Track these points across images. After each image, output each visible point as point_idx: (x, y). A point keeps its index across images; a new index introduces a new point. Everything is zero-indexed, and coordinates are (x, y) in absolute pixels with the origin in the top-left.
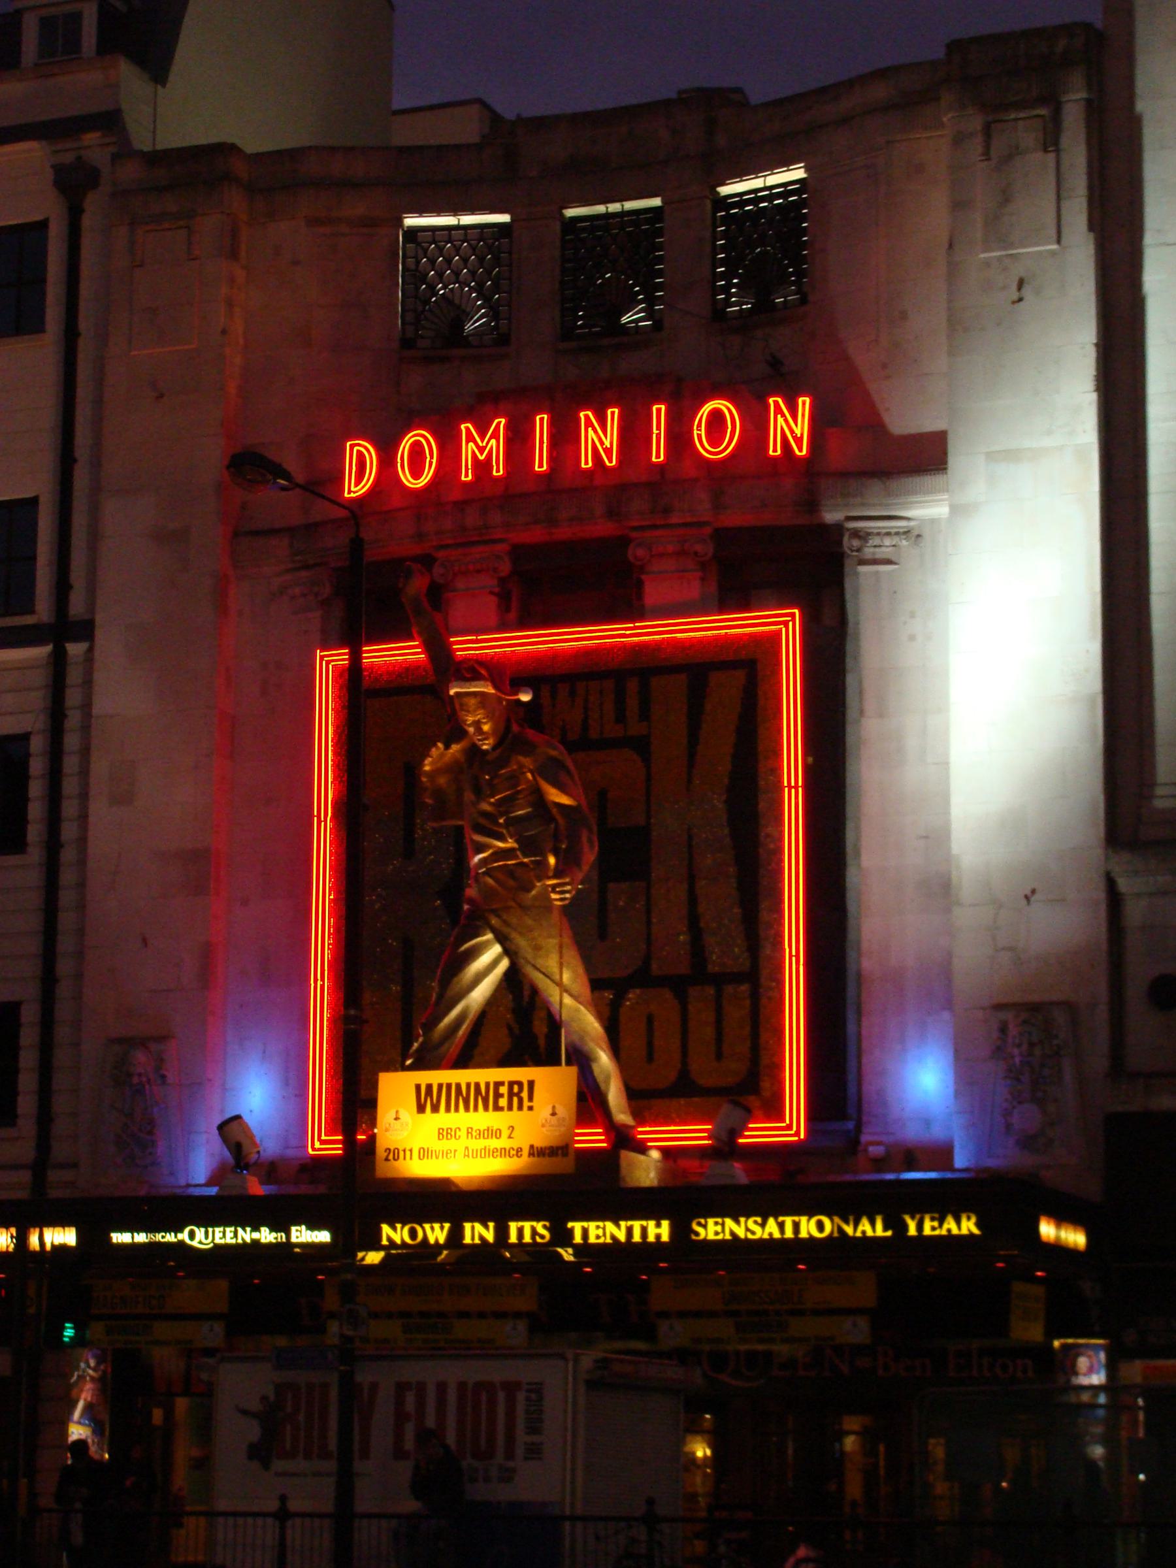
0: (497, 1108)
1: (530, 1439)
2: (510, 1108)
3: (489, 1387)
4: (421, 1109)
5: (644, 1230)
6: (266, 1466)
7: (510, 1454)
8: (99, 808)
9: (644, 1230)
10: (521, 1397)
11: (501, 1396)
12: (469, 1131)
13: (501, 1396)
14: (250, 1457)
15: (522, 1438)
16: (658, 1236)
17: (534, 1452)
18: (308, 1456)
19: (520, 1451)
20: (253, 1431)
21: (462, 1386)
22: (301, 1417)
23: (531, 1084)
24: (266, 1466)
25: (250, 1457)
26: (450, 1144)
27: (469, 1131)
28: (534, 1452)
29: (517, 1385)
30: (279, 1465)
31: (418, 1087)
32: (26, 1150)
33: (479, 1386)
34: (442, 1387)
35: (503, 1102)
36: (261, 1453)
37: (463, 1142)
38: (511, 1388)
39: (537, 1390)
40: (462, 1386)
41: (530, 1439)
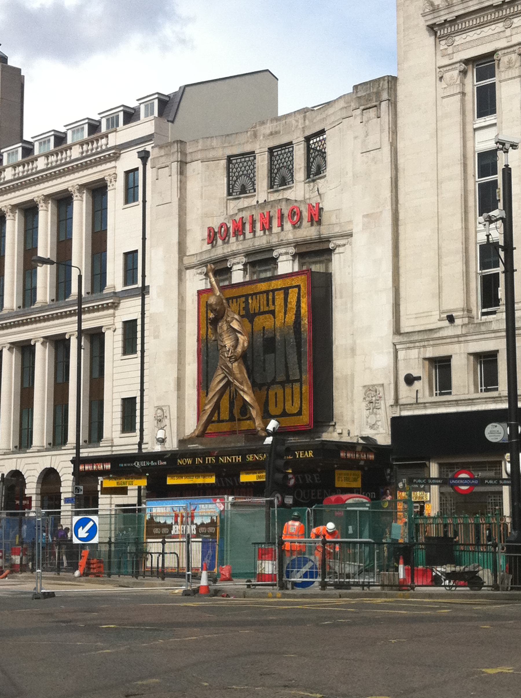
5: (235, 458)
9: (235, 458)
32: (137, 440)
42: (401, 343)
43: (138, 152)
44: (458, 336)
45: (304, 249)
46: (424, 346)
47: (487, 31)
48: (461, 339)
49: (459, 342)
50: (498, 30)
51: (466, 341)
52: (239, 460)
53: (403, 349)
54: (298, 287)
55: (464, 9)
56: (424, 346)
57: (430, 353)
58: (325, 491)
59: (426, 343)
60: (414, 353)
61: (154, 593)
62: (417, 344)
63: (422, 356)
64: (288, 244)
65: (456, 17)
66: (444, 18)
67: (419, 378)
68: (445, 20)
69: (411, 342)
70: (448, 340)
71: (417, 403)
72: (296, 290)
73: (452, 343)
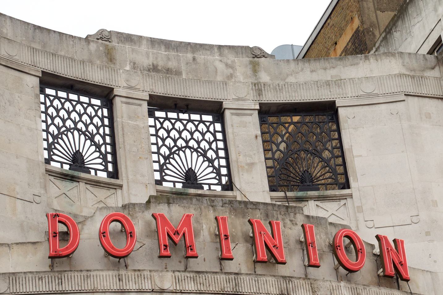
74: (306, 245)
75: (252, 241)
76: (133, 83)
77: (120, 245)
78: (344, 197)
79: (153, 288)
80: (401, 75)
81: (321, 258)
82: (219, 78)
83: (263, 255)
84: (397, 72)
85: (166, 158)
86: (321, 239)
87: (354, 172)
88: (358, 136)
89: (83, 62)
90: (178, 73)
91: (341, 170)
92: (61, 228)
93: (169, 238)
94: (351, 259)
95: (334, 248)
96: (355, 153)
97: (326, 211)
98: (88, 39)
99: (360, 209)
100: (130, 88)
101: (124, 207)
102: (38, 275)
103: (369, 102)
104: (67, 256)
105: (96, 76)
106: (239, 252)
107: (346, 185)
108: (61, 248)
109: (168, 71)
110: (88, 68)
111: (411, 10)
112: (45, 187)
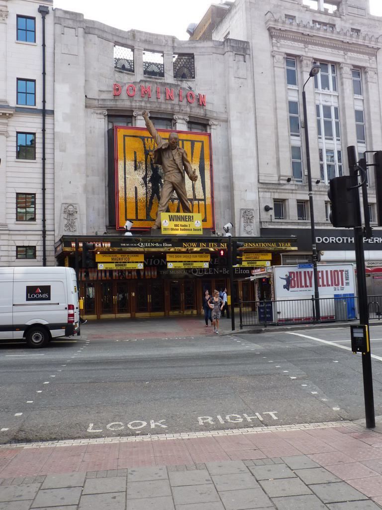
0: (186, 221)
1: (346, 281)
2: (189, 221)
3: (337, 271)
4: (170, 220)
5: (347, 240)
6: (288, 289)
7: (342, 285)
8: (57, 153)
9: (347, 240)
10: (344, 273)
11: (340, 273)
12: (181, 225)
13: (340, 273)
14: (284, 288)
15: (345, 281)
16: (351, 241)
17: (347, 284)
18: (298, 287)
19: (345, 284)
20: (285, 282)
21: (331, 271)
22: (296, 279)
23: (193, 216)
24: (288, 289)
25: (284, 288)
26: (177, 228)
27: (181, 225)
28: (347, 284)
29: (343, 271)
30: (291, 289)
31: (169, 216)
32: (40, 227)
33: (335, 271)
34: (327, 272)
35: (187, 220)
36: (287, 287)
37: (179, 228)
38: (342, 271)
39: (347, 271)
40: (331, 271)
41: (346, 281)
42: (262, 188)
43: (40, 6)
44: (292, 190)
45: (193, 120)
46: (274, 192)
47: (296, 44)
48: (294, 192)
49: (292, 193)
50: (301, 46)
51: (296, 193)
52: (351, 241)
53: (262, 192)
54: (125, 136)
55: (324, 35)
56: (274, 192)
57: (277, 196)
58: (215, 269)
59: (275, 191)
60: (268, 195)
61: (25, 353)
62: (271, 190)
63: (272, 197)
64: (185, 114)
65: (286, 30)
66: (280, 28)
67: (271, 209)
68: (308, 34)
69: (268, 189)
70: (287, 191)
71: (271, 222)
72: (200, 144)
73: (289, 193)
74: (179, 95)
75: (165, 93)
76: (140, 45)
77: (131, 93)
78: (193, 81)
79: (212, 127)
80: (212, 47)
81: (183, 99)
82: (163, 44)
83: (168, 98)
84: (211, 46)
85: (147, 67)
86: (183, 94)
87: (197, 74)
88: (200, 65)
89: (126, 38)
90: (152, 42)
91: (193, 70)
92: (117, 87)
93: (323, 344)
94: (190, 99)
95: (187, 96)
96: (197, 68)
97: (185, 85)
98: (128, 32)
99: (197, 85)
100: (139, 46)
101: (134, 82)
102: (111, 100)
103: (203, 54)
104: (118, 95)
105: (130, 43)
106: (162, 97)
107: (194, 78)
108: (117, 93)
109: (150, 41)
110: (128, 40)
111: (224, 21)
112: (114, 75)
